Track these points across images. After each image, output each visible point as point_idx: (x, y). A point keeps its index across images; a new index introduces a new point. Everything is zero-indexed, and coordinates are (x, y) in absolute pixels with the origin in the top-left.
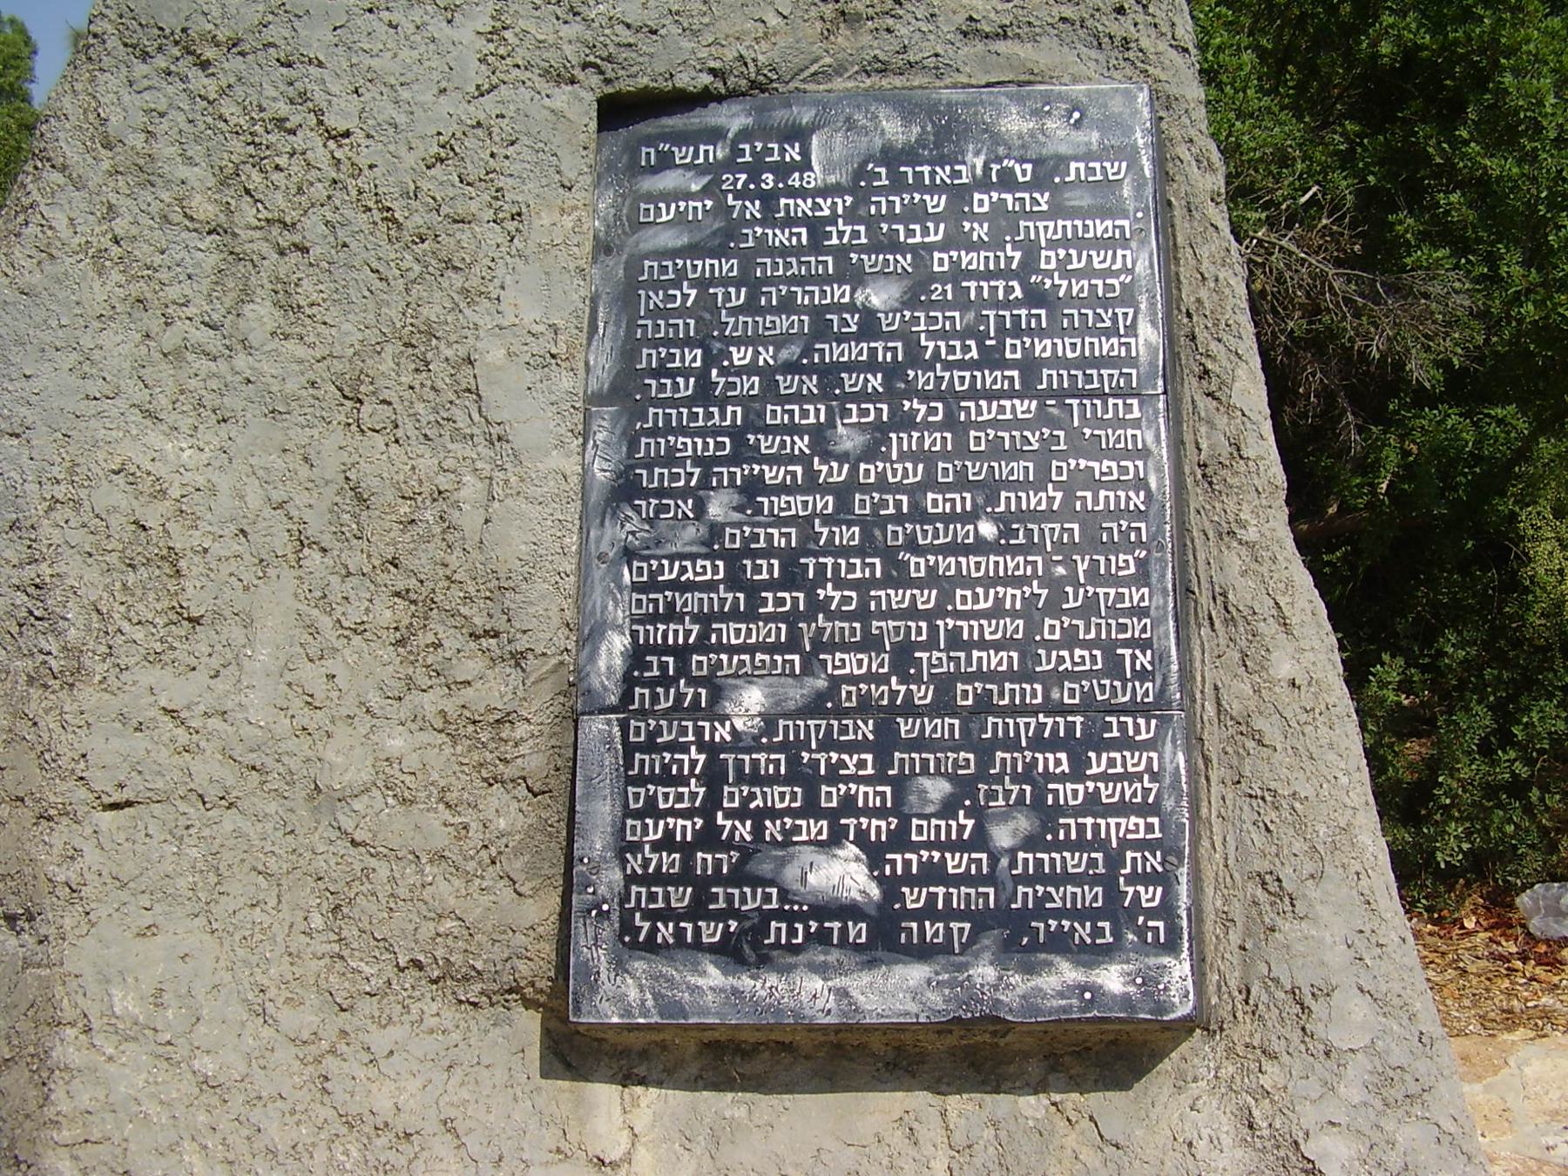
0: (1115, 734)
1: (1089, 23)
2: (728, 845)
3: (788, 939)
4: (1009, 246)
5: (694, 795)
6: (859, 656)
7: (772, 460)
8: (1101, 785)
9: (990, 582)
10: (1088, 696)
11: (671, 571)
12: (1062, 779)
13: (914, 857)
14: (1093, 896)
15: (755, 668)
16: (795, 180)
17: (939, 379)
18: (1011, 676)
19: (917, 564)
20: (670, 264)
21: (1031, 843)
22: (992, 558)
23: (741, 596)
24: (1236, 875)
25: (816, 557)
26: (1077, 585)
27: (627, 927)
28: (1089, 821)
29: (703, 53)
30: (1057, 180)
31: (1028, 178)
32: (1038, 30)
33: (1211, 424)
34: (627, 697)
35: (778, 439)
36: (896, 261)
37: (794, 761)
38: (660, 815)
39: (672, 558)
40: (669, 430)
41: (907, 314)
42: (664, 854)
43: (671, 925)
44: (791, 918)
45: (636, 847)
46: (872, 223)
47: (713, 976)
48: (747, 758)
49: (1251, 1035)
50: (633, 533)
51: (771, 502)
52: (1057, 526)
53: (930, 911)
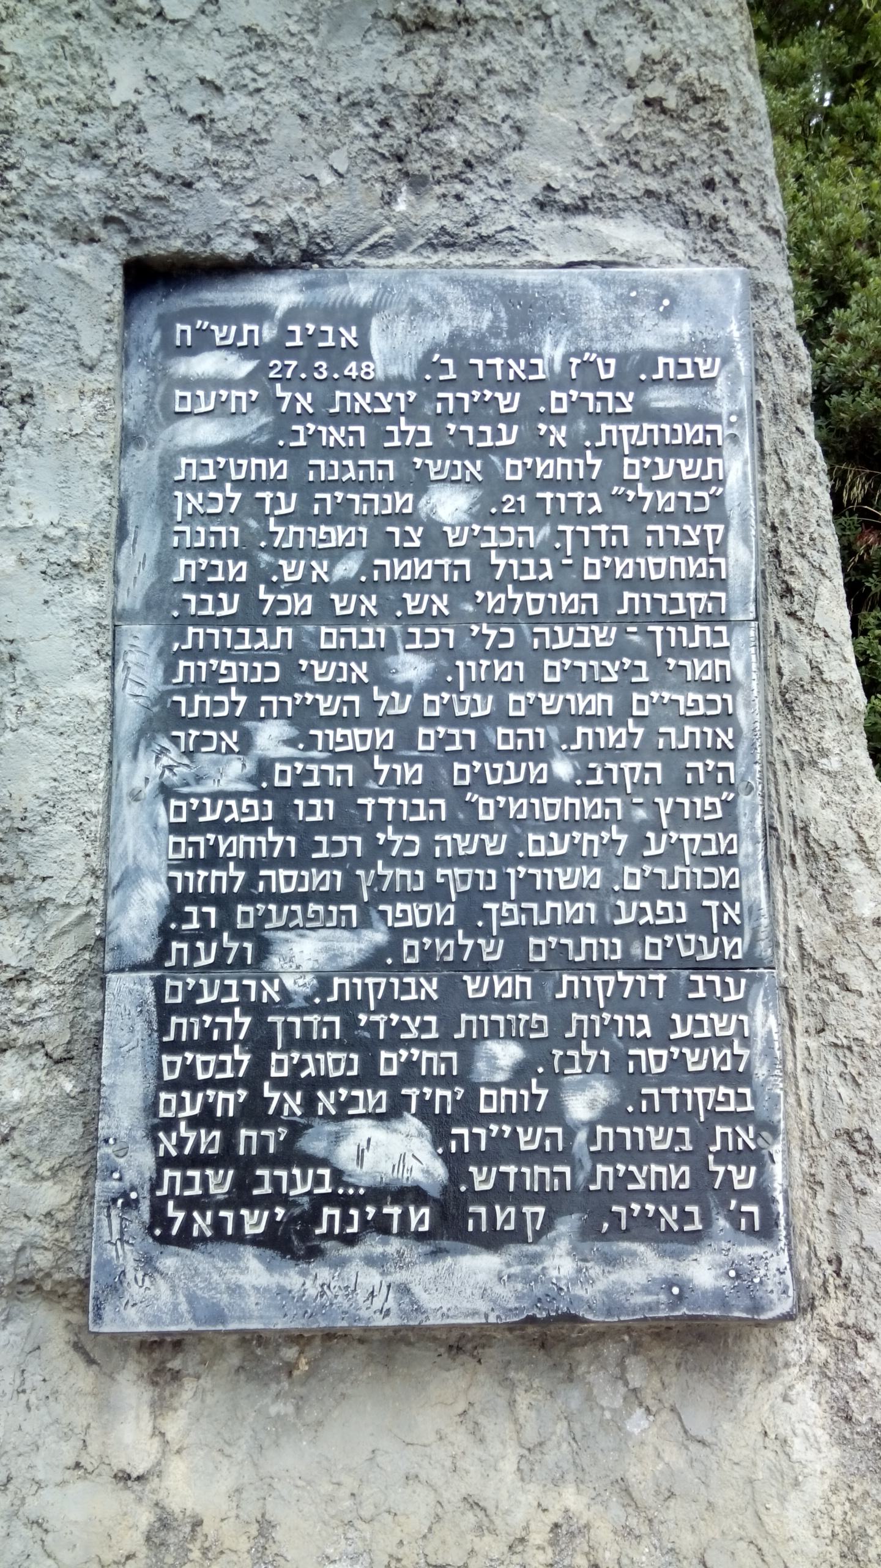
0: (701, 994)
1: (677, 198)
2: (274, 1121)
3: (342, 1229)
4: (589, 453)
5: (237, 1064)
6: (423, 907)
7: (325, 688)
8: (686, 1050)
9: (563, 826)
10: (671, 951)
11: (214, 810)
12: (644, 1043)
13: (482, 1131)
14: (678, 1175)
15: (306, 919)
16: (351, 369)
17: (511, 602)
18: (588, 929)
19: (486, 806)
20: (210, 462)
21: (611, 1115)
22: (568, 800)
23: (292, 839)
24: (823, 1133)
25: (376, 797)
26: (660, 830)
27: (158, 1216)
28: (674, 1091)
29: (246, 214)
30: (643, 377)
31: (611, 375)
32: (621, 204)
33: (793, 646)
34: (163, 952)
35: (334, 665)
36: (465, 467)
37: (350, 1024)
38: (198, 1087)
39: (215, 796)
40: (208, 652)
41: (477, 528)
42: (203, 1132)
43: (209, 1214)
44: (344, 1203)
45: (170, 1125)
46: (438, 421)
47: (254, 1271)
48: (297, 1020)
49: (845, 1314)
50: (170, 768)
51: (326, 736)
52: (638, 766)
53: (499, 1194)
